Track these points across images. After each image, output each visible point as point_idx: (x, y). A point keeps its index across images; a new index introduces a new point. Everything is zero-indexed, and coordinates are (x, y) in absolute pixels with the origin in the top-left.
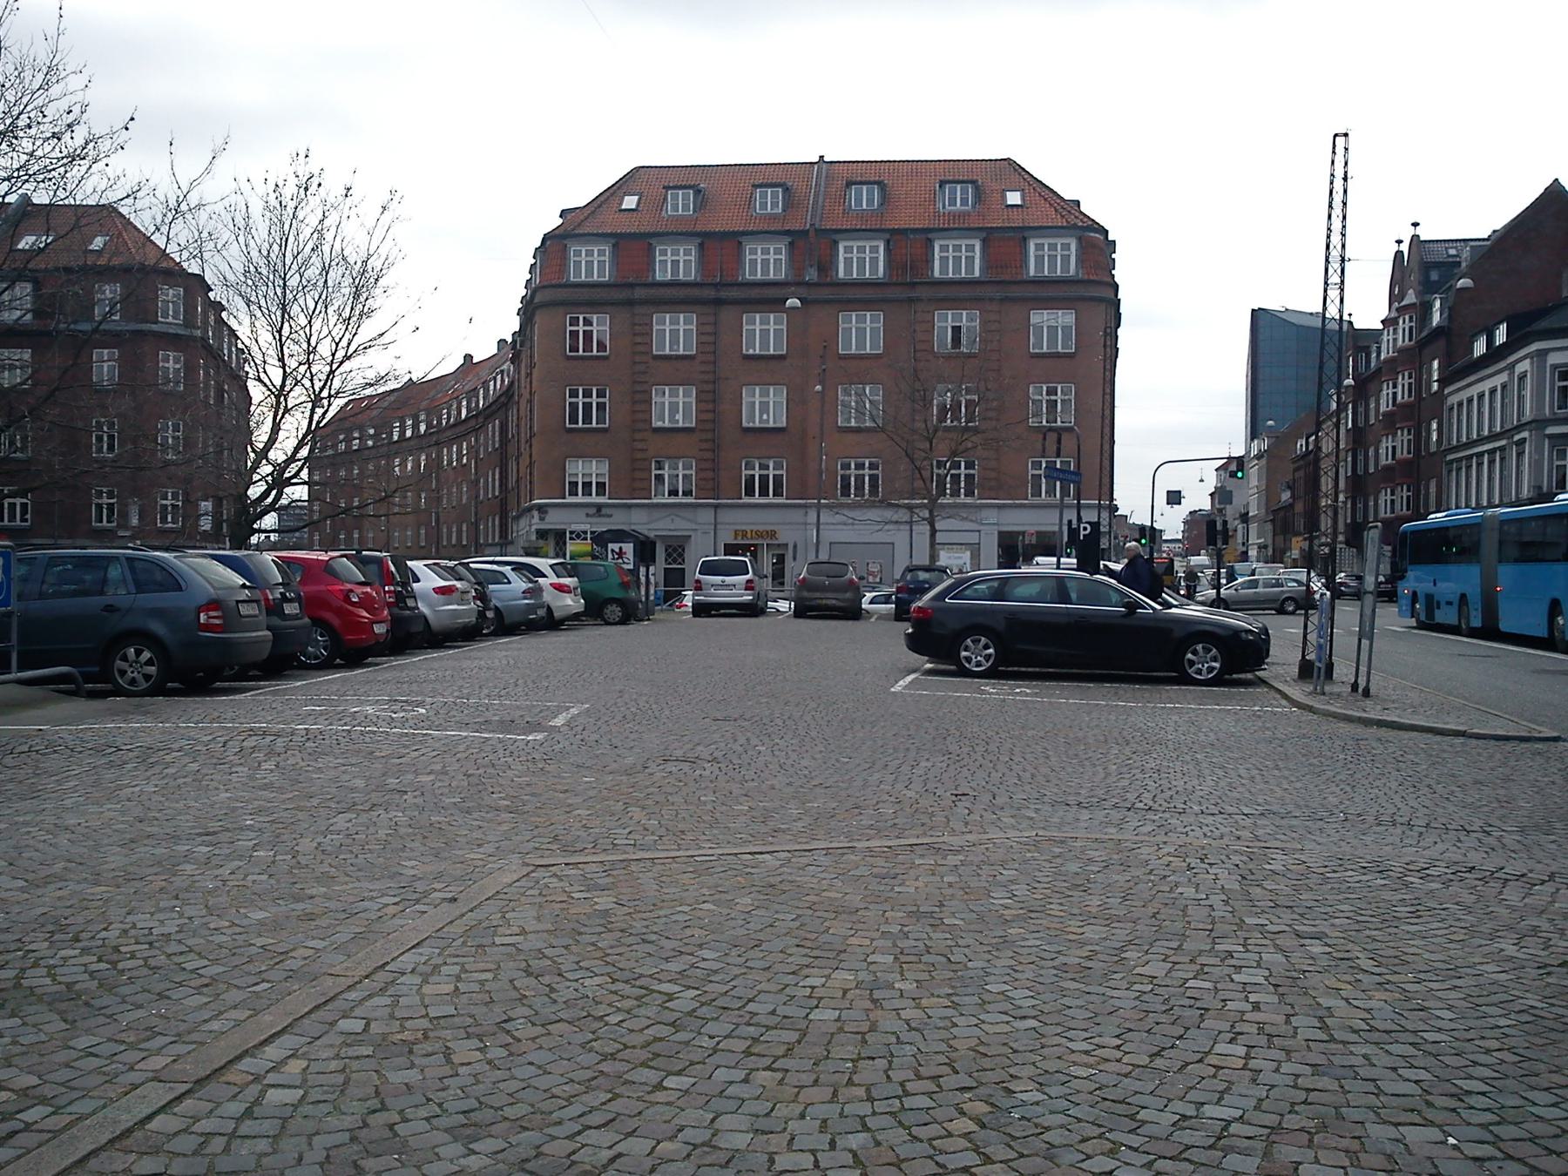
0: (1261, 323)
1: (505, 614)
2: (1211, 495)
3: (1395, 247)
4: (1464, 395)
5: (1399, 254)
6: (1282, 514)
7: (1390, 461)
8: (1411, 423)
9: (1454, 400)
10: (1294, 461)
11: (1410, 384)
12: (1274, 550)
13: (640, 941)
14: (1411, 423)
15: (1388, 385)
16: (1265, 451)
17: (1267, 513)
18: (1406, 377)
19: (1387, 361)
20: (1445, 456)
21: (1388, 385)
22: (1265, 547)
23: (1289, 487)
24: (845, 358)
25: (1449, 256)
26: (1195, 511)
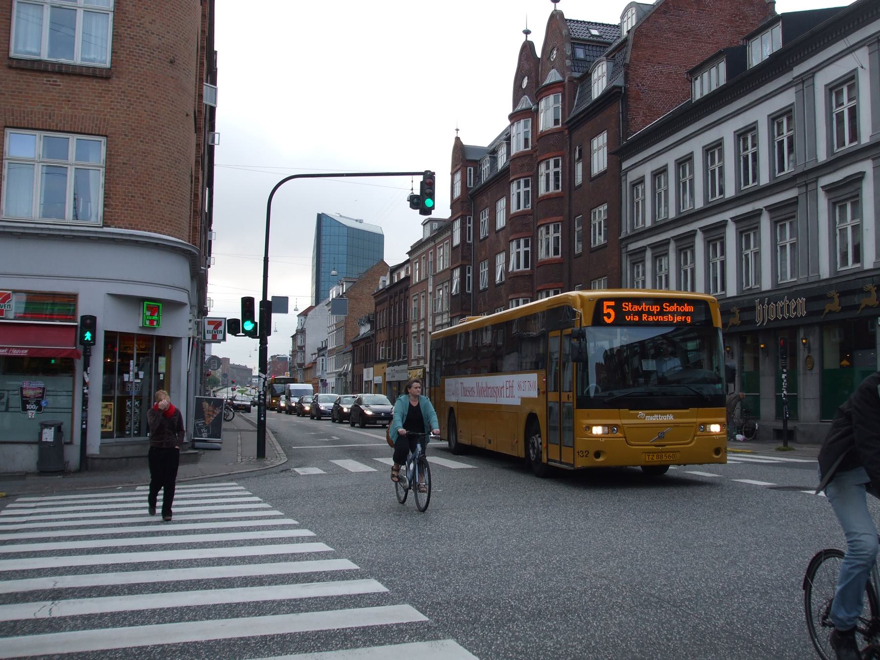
0: (323, 224)
1: (148, 467)
2: (292, 337)
3: (522, 38)
4: (647, 170)
5: (527, 48)
6: (362, 344)
7: (522, 268)
8: (559, 218)
9: (633, 176)
10: (376, 296)
11: (556, 174)
12: (353, 376)
13: (625, 182)
14: (559, 218)
15: (519, 183)
16: (343, 293)
17: (346, 342)
18: (522, 185)
19: (520, 156)
20: (626, 246)
21: (519, 183)
22: (345, 375)
23: (369, 321)
24: (69, 74)
25: (593, 36)
26: (275, 356)
